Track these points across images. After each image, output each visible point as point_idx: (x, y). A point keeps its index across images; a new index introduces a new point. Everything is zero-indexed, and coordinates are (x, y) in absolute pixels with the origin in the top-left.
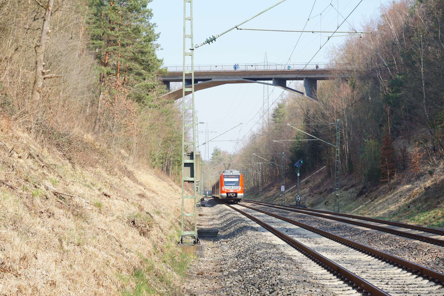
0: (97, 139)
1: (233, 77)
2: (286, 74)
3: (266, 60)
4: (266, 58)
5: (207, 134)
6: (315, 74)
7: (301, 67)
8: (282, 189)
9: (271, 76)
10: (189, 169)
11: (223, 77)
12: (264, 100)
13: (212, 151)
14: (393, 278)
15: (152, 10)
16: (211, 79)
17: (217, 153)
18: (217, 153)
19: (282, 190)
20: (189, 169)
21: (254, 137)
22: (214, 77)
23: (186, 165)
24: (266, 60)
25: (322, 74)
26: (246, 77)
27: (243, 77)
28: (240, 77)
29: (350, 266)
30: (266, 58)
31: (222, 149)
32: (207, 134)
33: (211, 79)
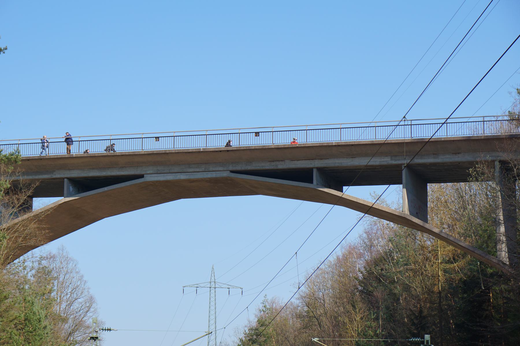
1: (203, 169)
2: (353, 156)
3: (213, 278)
4: (213, 275)
5: (213, 291)
6: (436, 154)
9: (307, 162)
11: (176, 169)
12: (209, 325)
14: (48, 148)
16: (142, 176)
22: (150, 170)
24: (213, 278)
25: (456, 154)
26: (239, 168)
27: (231, 168)
28: (221, 169)
30: (213, 275)
32: (213, 291)
33: (142, 176)
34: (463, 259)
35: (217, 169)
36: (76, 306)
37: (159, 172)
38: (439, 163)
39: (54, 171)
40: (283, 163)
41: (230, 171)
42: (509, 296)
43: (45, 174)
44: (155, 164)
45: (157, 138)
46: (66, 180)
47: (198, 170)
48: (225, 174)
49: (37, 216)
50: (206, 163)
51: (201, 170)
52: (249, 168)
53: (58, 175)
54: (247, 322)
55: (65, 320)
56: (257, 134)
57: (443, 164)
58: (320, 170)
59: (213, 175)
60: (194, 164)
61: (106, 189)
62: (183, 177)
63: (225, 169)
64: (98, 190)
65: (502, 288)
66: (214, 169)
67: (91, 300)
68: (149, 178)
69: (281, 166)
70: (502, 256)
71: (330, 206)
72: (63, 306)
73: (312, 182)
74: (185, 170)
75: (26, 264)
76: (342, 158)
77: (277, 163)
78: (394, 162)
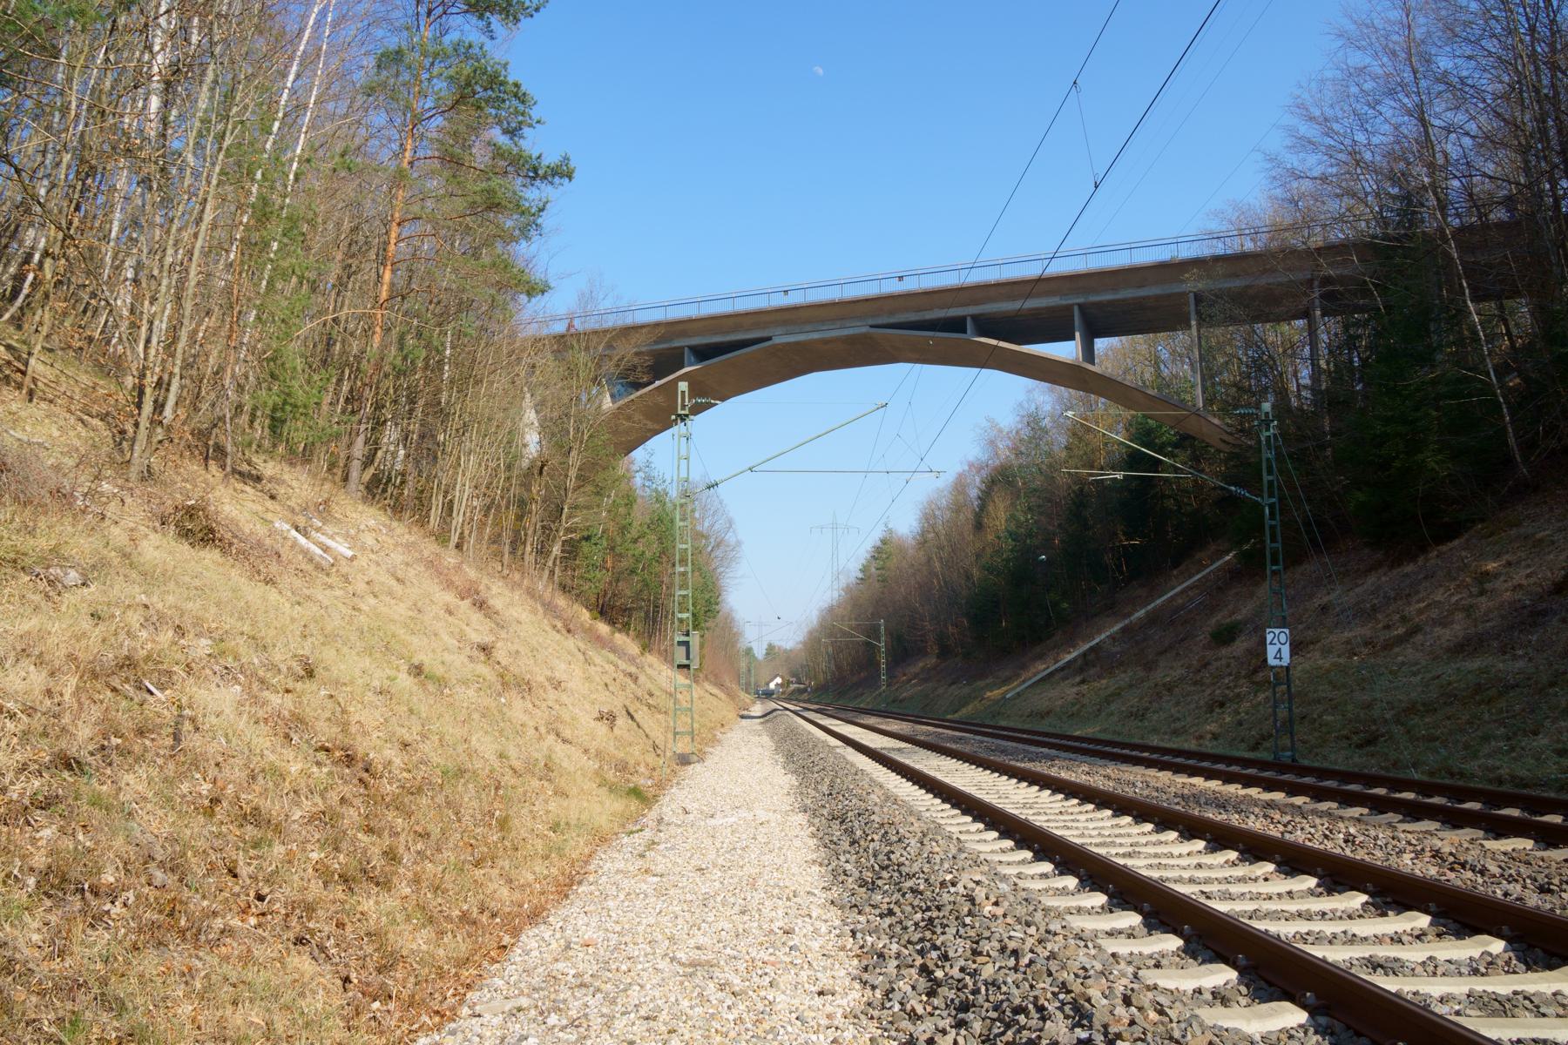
0: (474, 670)
7: (1031, 271)
8: (1271, 651)
10: (683, 649)
11: (808, 328)
13: (765, 646)
15: (566, 159)
16: (769, 339)
17: (771, 648)
18: (771, 648)
19: (1272, 661)
20: (683, 649)
21: (831, 609)
22: (779, 331)
23: (680, 643)
26: (880, 321)
27: (871, 322)
29: (1414, 954)
31: (777, 643)
33: (769, 339)
34: (1050, 466)
36: (717, 527)
38: (1118, 300)
44: (785, 323)
45: (786, 292)
48: (864, 330)
53: (676, 344)
55: (707, 538)
56: (901, 278)
57: (1124, 300)
58: (975, 318)
59: (850, 332)
62: (816, 336)
67: (730, 523)
68: (777, 340)
70: (749, 651)
71: (975, 370)
72: (706, 524)
73: (965, 332)
75: (872, 817)
78: (1064, 302)
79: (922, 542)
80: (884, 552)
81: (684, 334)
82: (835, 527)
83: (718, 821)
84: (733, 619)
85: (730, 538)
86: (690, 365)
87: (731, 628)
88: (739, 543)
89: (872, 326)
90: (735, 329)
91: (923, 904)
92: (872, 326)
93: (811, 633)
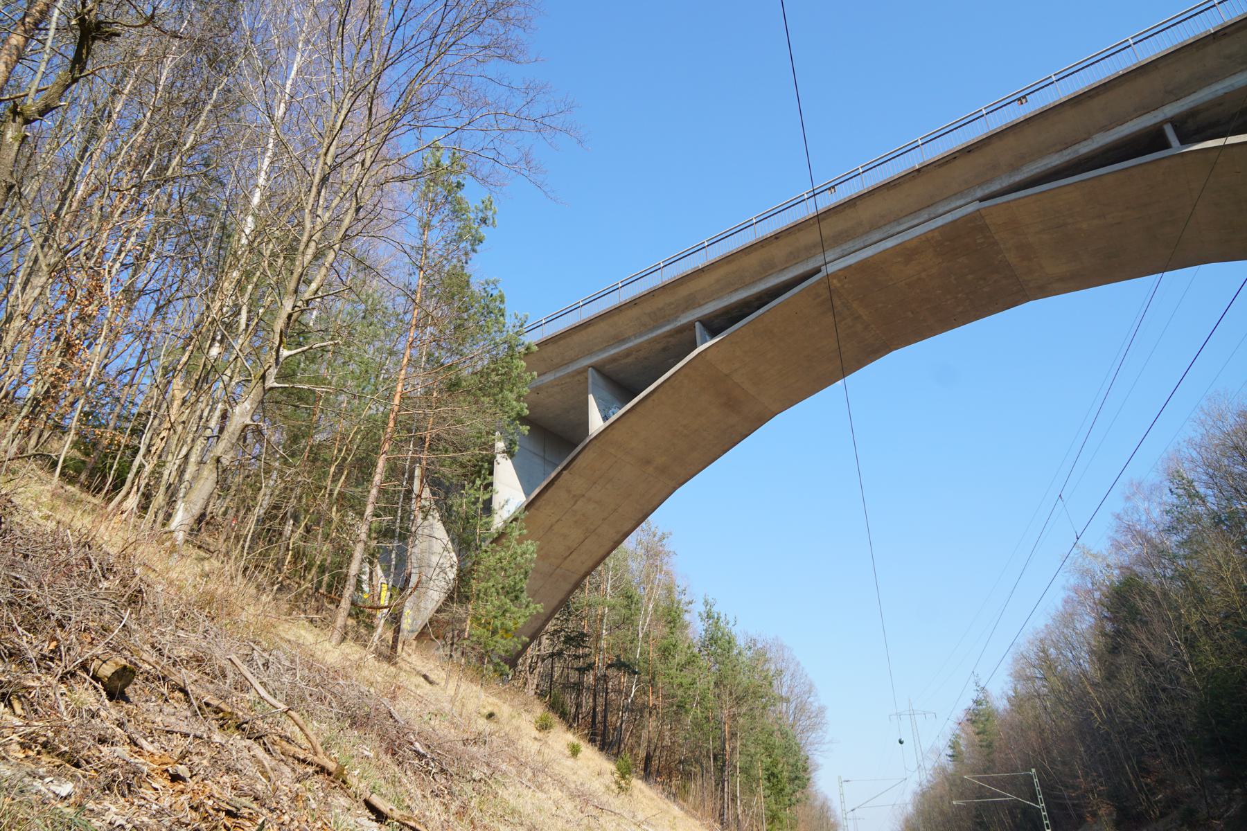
11: (876, 236)
16: (818, 271)
26: (995, 187)
27: (980, 193)
33: (818, 271)
35: (953, 205)
37: (845, 253)
39: (679, 317)
40: (1089, 142)
41: (978, 200)
42: (204, 644)
43: (665, 325)
46: (697, 324)
47: (916, 222)
49: (491, 461)
50: (929, 206)
51: (922, 220)
52: (1018, 178)
53: (684, 320)
54: (672, 549)
55: (787, 700)
58: (1173, 121)
60: (906, 216)
61: (761, 311)
62: (889, 244)
63: (969, 199)
64: (1166, 151)
65: (85, 675)
66: (947, 208)
68: (832, 268)
69: (1085, 148)
73: (1167, 145)
74: (891, 232)
76: (1231, 75)
77: (1077, 147)
79: (1018, 703)
80: (979, 718)
81: (691, 302)
82: (912, 714)
83: (338, 199)
84: (829, 808)
85: (814, 703)
86: (704, 341)
87: (828, 819)
88: (822, 710)
89: (981, 200)
90: (768, 268)
91: (411, 709)
92: (981, 200)
93: (907, 820)
